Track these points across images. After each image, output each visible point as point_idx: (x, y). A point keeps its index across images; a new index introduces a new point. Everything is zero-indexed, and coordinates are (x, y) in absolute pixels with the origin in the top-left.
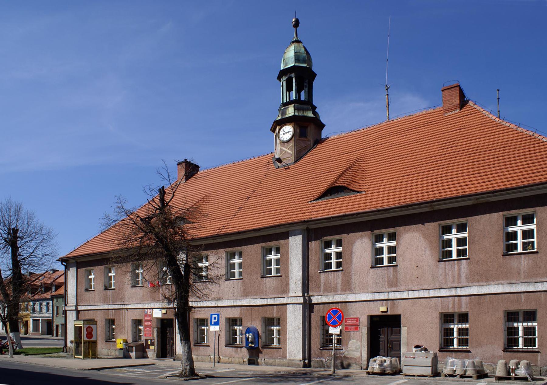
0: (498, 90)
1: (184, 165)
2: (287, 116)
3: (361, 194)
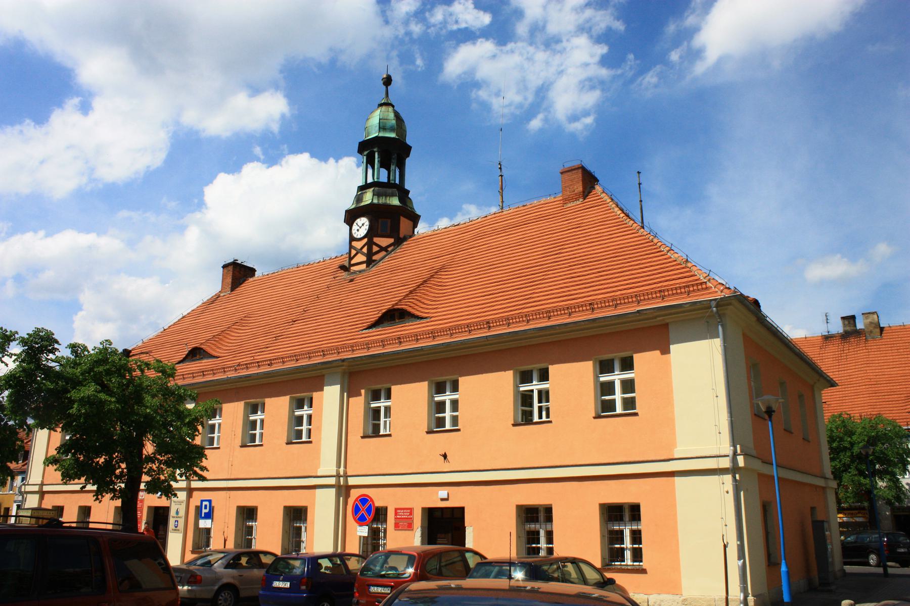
0: (639, 173)
1: (231, 268)
2: (362, 204)
3: (425, 321)
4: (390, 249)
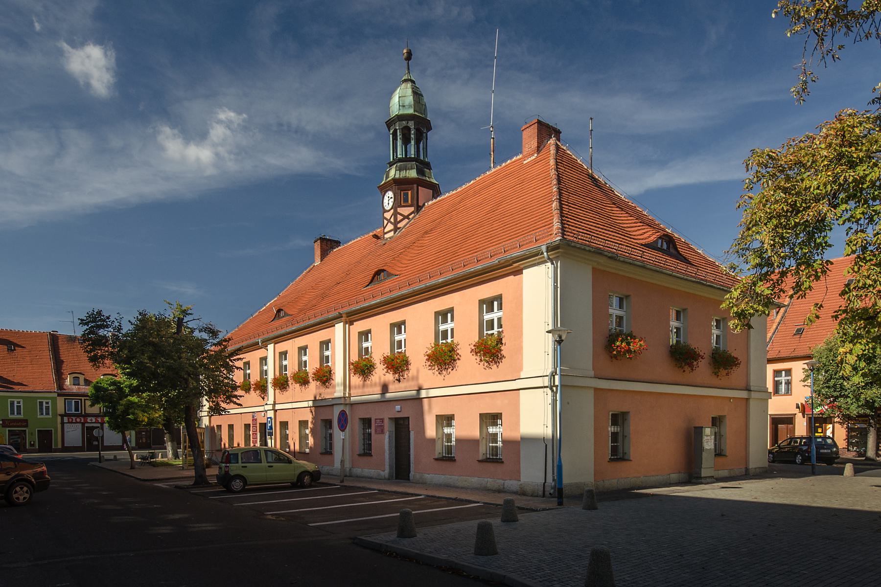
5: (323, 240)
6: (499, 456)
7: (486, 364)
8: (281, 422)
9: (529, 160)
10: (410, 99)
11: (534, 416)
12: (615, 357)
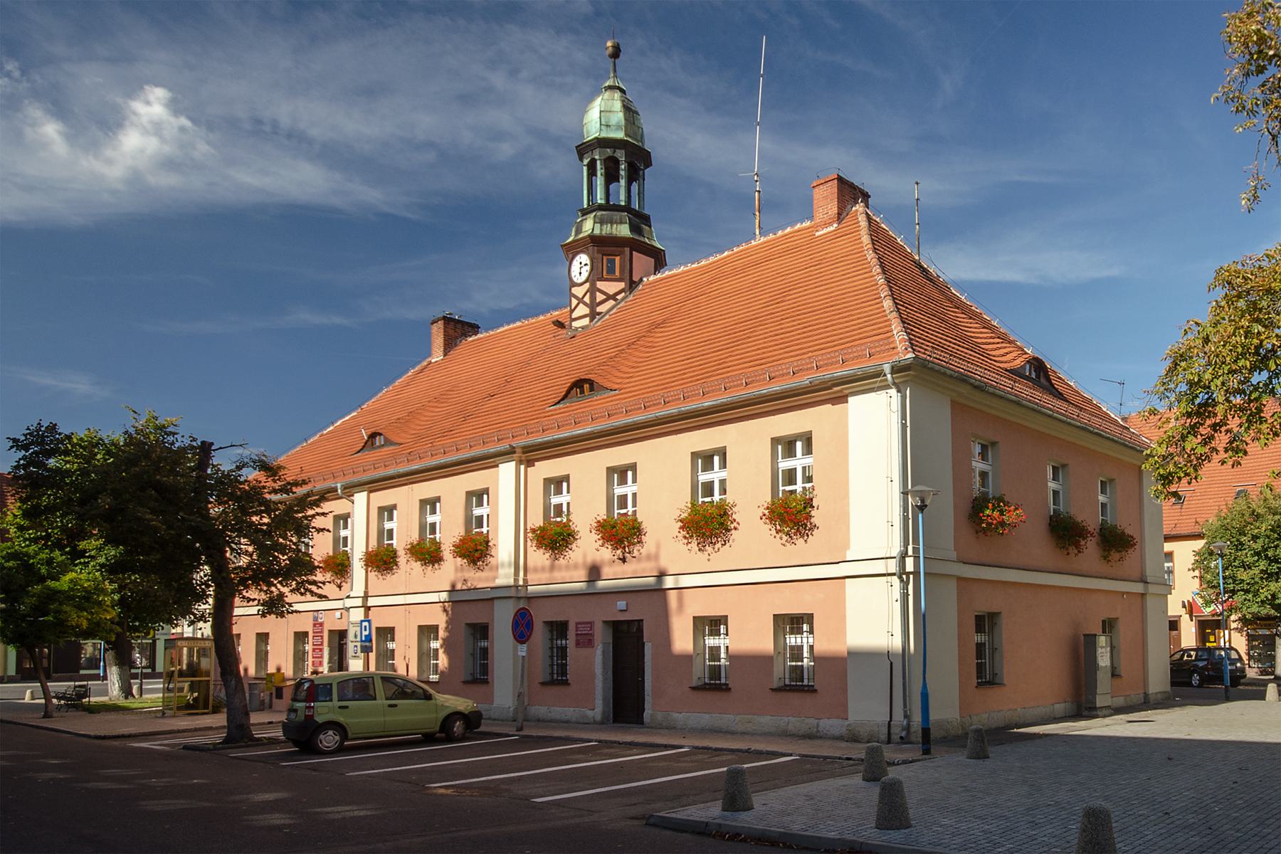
4: (619, 297)
5: (448, 320)
6: (803, 682)
7: (785, 538)
8: (330, 631)
9: (825, 231)
10: (618, 117)
11: (872, 619)
12: (984, 531)
